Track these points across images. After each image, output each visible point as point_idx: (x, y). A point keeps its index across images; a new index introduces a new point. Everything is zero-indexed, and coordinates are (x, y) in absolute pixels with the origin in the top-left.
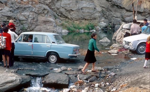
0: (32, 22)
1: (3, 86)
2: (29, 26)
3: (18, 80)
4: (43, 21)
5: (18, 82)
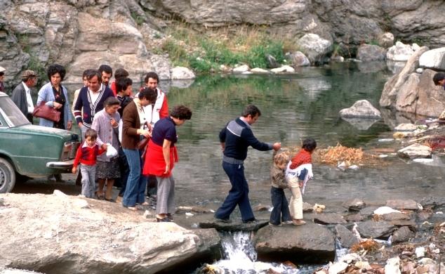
0: (62, 40)
1: (150, 259)
2: (50, 56)
3: (193, 242)
4: (98, 34)
5: (191, 246)
